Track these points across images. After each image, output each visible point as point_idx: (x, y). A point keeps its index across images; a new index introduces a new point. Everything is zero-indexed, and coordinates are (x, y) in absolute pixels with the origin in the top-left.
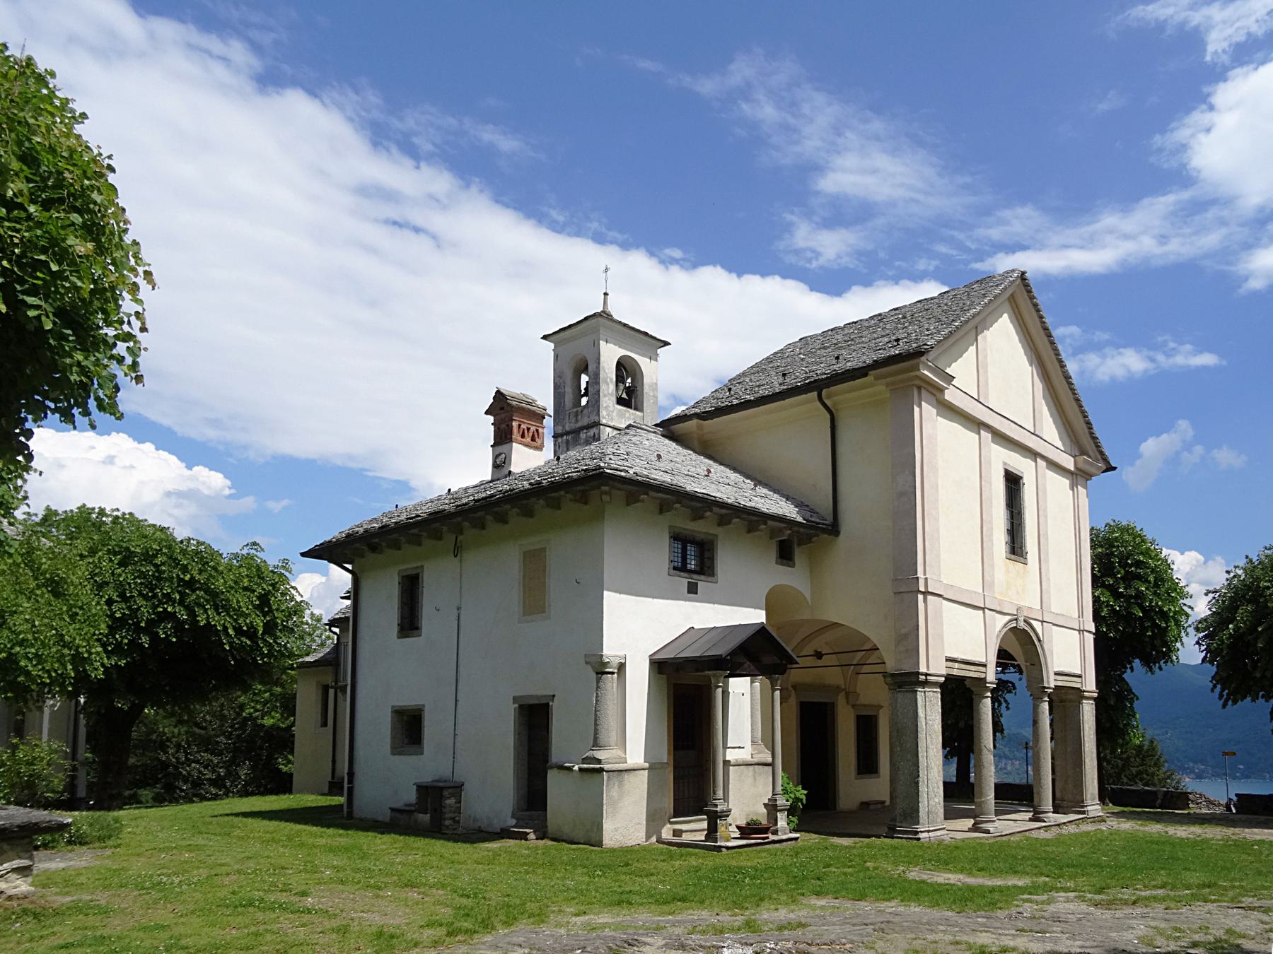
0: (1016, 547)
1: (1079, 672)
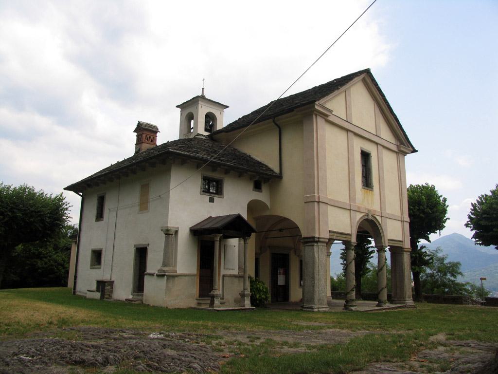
0: (367, 182)
1: (401, 239)
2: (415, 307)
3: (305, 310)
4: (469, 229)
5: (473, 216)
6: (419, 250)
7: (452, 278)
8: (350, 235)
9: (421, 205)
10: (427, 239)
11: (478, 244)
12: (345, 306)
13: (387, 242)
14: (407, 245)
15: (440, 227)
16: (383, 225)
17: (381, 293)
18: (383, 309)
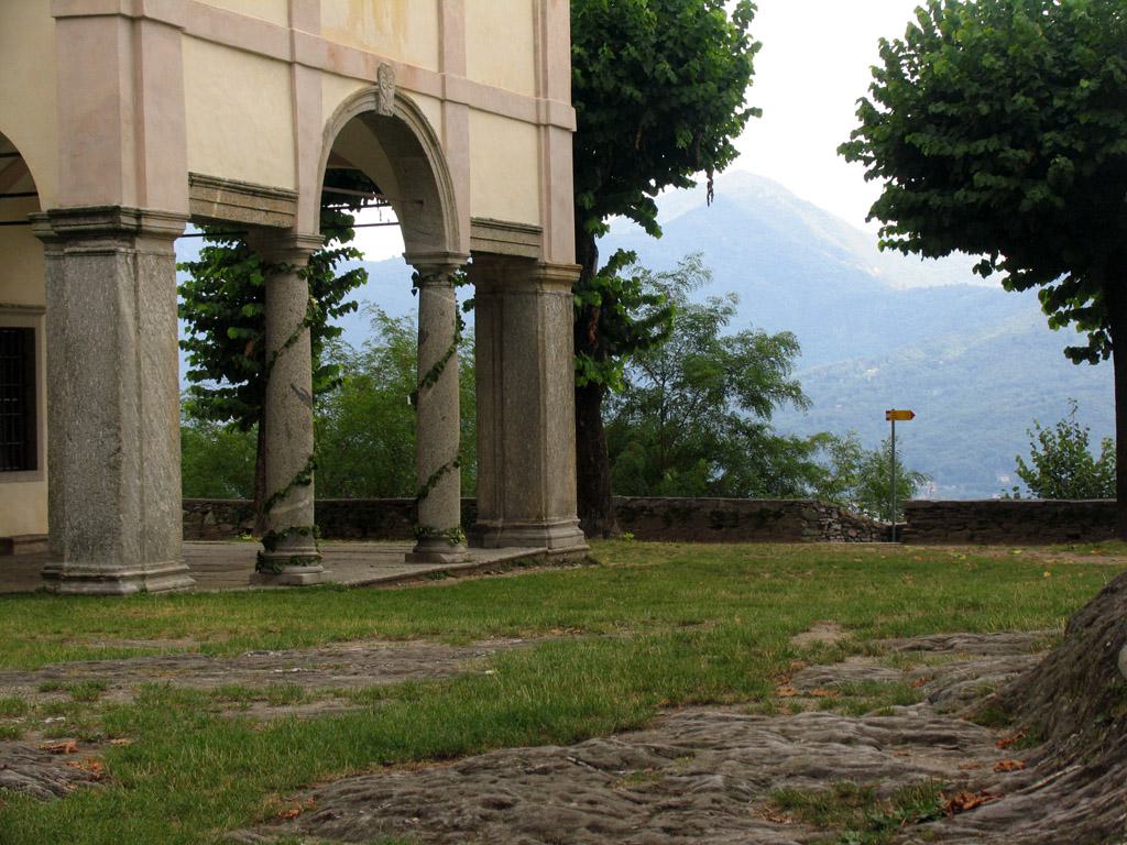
2: (589, 561)
3: (73, 588)
4: (859, 168)
5: (881, 108)
6: (605, 271)
7: (748, 416)
8: (291, 197)
9: (630, 39)
10: (646, 216)
11: (893, 245)
12: (263, 562)
13: (465, 231)
14: (560, 250)
15: (715, 156)
16: (450, 146)
17: (433, 491)
18: (446, 573)
